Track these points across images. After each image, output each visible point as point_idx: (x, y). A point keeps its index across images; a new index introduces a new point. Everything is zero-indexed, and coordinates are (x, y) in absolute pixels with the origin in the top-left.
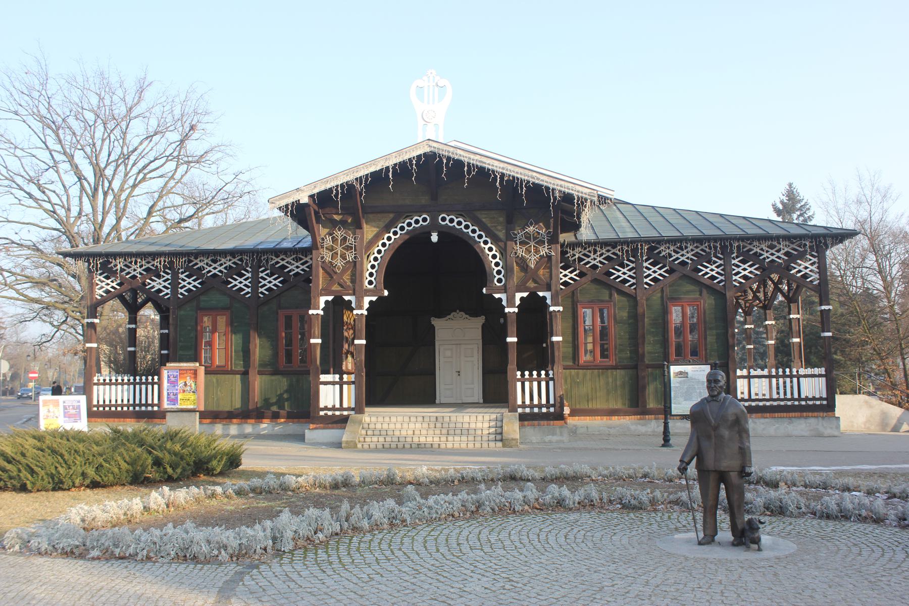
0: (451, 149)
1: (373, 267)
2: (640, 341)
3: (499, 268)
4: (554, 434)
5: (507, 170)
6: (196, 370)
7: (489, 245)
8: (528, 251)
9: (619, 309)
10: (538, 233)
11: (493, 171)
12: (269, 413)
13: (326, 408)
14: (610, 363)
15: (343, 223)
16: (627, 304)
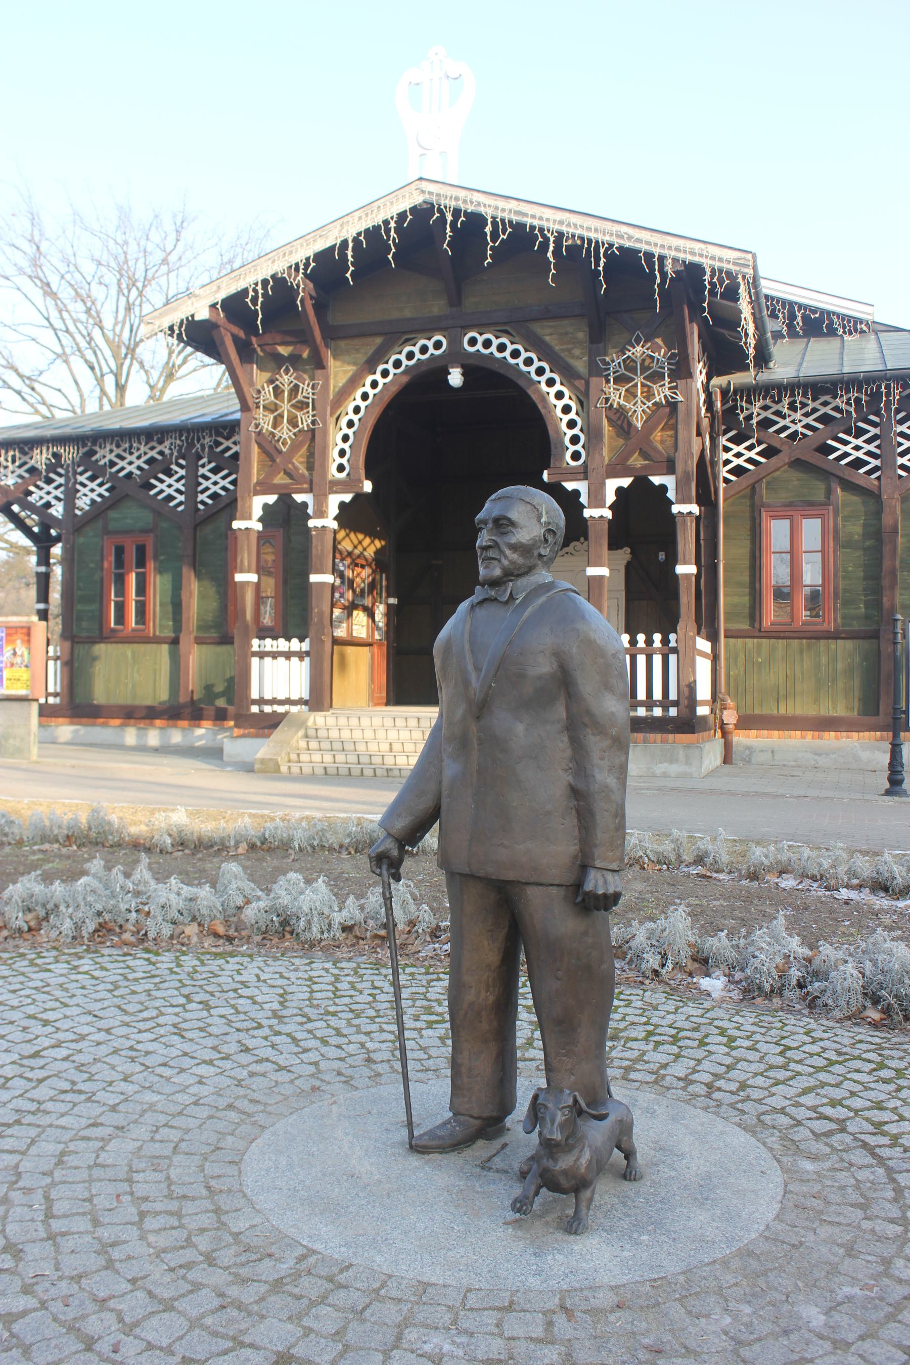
0: (462, 194)
1: (345, 438)
2: (886, 582)
3: (576, 431)
4: (672, 760)
5: (569, 225)
6: (29, 629)
7: (558, 387)
8: (631, 394)
9: (845, 519)
10: (652, 358)
11: (541, 230)
12: (210, 711)
13: (261, 701)
14: (825, 627)
15: (294, 361)
16: (862, 508)
